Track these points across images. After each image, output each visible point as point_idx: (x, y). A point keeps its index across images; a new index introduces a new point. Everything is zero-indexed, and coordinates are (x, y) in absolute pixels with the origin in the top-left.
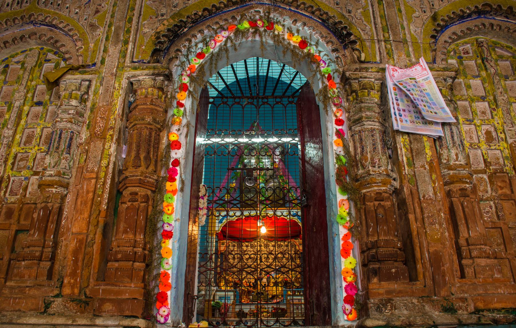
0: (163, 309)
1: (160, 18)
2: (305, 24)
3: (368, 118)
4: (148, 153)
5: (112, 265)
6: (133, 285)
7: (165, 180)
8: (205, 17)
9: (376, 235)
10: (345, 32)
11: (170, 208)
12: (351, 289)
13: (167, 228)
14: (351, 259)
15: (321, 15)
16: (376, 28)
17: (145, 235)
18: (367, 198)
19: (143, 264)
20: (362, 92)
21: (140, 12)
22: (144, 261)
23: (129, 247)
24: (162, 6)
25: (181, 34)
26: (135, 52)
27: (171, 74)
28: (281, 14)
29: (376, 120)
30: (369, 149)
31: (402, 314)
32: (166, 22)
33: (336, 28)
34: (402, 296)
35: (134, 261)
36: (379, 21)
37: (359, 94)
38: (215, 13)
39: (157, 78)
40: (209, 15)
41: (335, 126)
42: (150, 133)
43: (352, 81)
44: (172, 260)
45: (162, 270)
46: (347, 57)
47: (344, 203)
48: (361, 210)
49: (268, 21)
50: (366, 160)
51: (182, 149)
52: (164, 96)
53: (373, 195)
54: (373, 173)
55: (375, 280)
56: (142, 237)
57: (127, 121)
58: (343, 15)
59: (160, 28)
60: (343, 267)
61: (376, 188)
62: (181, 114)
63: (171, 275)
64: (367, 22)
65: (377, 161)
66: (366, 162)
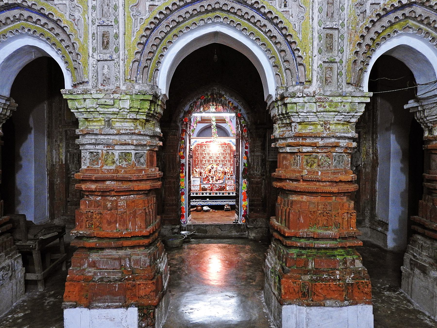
14: (246, 202)
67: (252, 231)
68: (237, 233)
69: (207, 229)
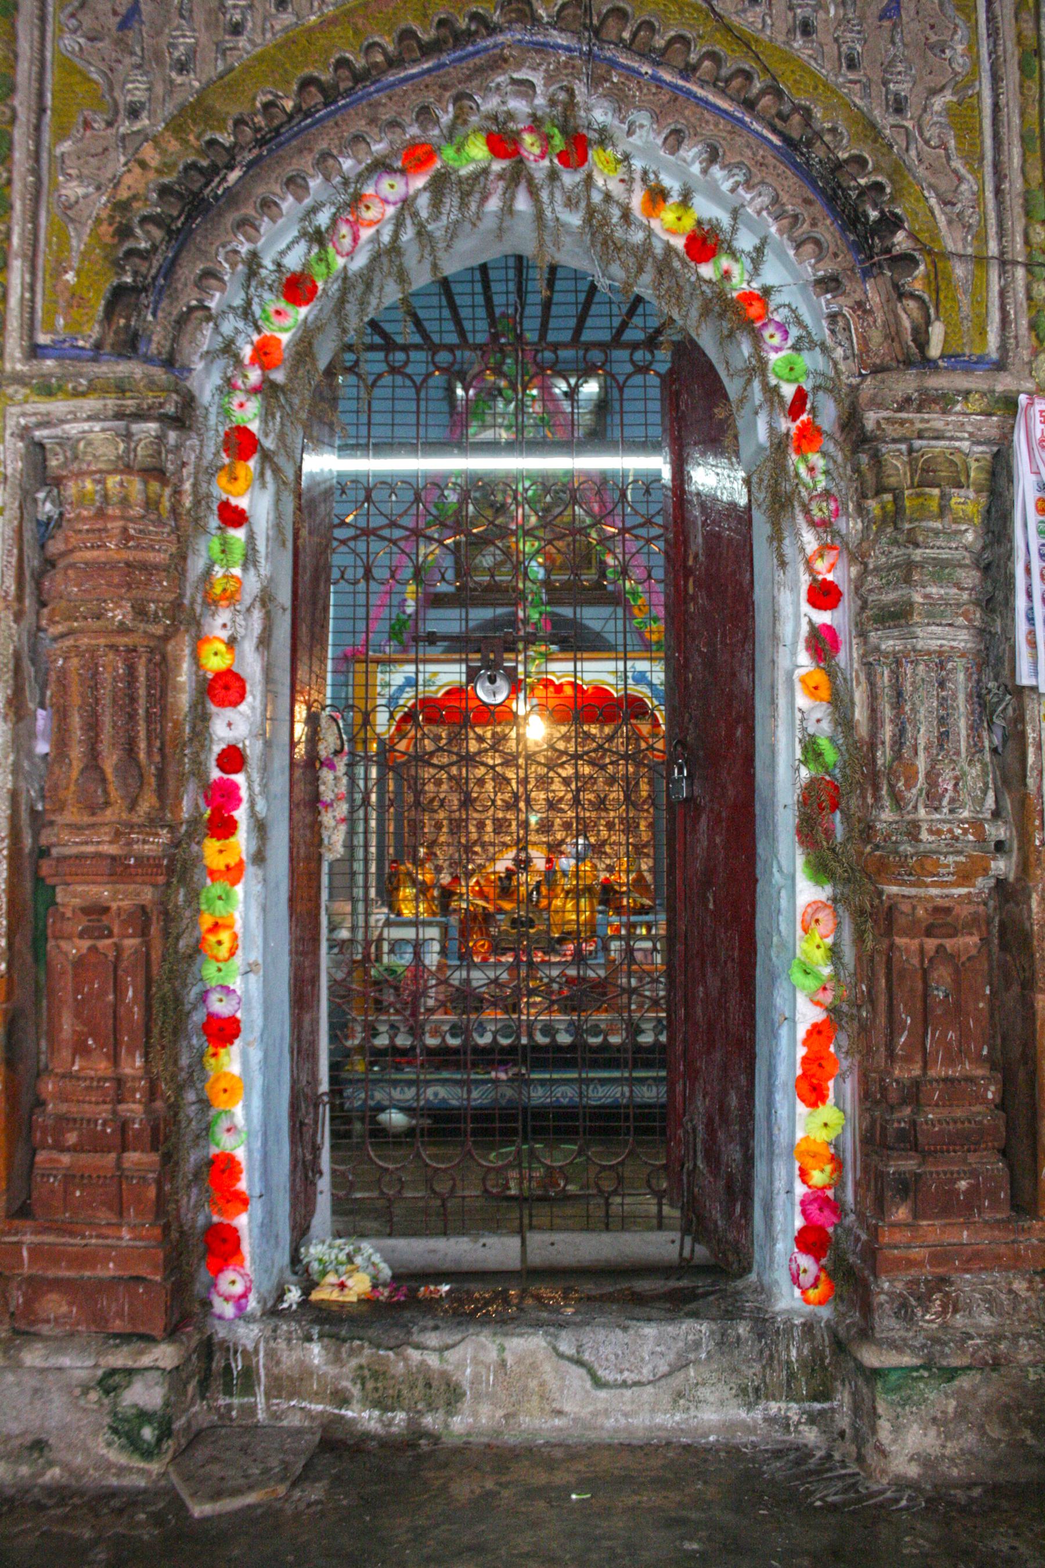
0: (229, 1275)
1: (125, 127)
2: (713, 156)
3: (934, 612)
4: (130, 750)
5: (51, 1160)
6: (126, 1234)
7: (197, 832)
8: (308, 114)
9: (919, 1058)
10: (874, 215)
11: (225, 936)
12: (821, 1209)
13: (220, 1006)
14: (828, 1112)
15: (784, 118)
16: (998, 192)
17: (146, 1055)
18: (902, 921)
19: (155, 1157)
20: (919, 495)
21: (41, 95)
22: (154, 1148)
23: (97, 1103)
24: (128, 61)
25: (217, 198)
26: (39, 298)
27: (189, 401)
28: (620, 101)
29: (961, 621)
30: (924, 734)
31: (976, 1326)
32: (149, 153)
33: (840, 186)
34: (981, 1269)
35: (124, 1149)
36: (1016, 161)
37: (907, 504)
38: (349, 92)
39: (135, 427)
40: (326, 105)
41: (805, 608)
42: (131, 669)
43: (884, 448)
44: (247, 1107)
45: (214, 1150)
46: (871, 312)
47: (820, 916)
48: (877, 958)
49: (563, 131)
50: (910, 781)
51: (249, 698)
52: (168, 491)
53: (921, 912)
54: (931, 838)
55: (902, 1213)
56: (139, 1062)
57: (43, 604)
58: (873, 126)
59: (128, 180)
60: (799, 1135)
61: (934, 891)
62: (238, 552)
63: (244, 1164)
64: (967, 159)
65: (950, 787)
66: (909, 786)
67: (905, 1402)
68: (750, 1407)
69: (461, 1365)
